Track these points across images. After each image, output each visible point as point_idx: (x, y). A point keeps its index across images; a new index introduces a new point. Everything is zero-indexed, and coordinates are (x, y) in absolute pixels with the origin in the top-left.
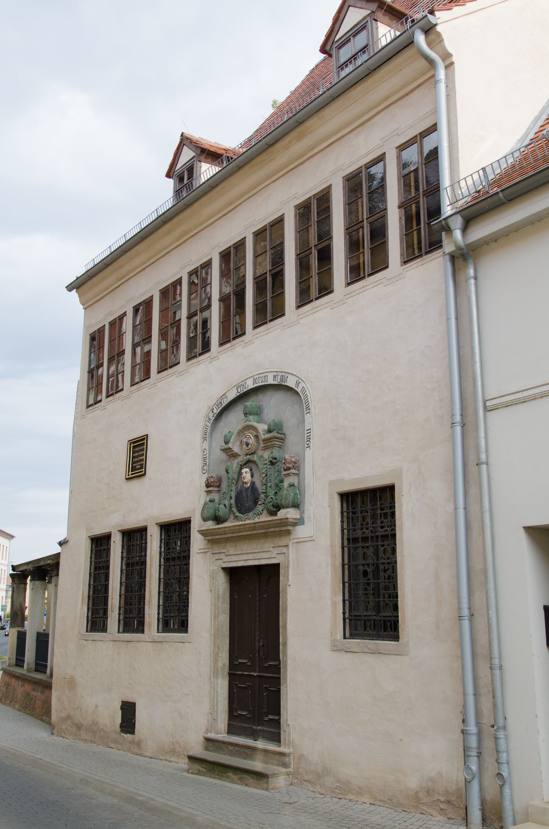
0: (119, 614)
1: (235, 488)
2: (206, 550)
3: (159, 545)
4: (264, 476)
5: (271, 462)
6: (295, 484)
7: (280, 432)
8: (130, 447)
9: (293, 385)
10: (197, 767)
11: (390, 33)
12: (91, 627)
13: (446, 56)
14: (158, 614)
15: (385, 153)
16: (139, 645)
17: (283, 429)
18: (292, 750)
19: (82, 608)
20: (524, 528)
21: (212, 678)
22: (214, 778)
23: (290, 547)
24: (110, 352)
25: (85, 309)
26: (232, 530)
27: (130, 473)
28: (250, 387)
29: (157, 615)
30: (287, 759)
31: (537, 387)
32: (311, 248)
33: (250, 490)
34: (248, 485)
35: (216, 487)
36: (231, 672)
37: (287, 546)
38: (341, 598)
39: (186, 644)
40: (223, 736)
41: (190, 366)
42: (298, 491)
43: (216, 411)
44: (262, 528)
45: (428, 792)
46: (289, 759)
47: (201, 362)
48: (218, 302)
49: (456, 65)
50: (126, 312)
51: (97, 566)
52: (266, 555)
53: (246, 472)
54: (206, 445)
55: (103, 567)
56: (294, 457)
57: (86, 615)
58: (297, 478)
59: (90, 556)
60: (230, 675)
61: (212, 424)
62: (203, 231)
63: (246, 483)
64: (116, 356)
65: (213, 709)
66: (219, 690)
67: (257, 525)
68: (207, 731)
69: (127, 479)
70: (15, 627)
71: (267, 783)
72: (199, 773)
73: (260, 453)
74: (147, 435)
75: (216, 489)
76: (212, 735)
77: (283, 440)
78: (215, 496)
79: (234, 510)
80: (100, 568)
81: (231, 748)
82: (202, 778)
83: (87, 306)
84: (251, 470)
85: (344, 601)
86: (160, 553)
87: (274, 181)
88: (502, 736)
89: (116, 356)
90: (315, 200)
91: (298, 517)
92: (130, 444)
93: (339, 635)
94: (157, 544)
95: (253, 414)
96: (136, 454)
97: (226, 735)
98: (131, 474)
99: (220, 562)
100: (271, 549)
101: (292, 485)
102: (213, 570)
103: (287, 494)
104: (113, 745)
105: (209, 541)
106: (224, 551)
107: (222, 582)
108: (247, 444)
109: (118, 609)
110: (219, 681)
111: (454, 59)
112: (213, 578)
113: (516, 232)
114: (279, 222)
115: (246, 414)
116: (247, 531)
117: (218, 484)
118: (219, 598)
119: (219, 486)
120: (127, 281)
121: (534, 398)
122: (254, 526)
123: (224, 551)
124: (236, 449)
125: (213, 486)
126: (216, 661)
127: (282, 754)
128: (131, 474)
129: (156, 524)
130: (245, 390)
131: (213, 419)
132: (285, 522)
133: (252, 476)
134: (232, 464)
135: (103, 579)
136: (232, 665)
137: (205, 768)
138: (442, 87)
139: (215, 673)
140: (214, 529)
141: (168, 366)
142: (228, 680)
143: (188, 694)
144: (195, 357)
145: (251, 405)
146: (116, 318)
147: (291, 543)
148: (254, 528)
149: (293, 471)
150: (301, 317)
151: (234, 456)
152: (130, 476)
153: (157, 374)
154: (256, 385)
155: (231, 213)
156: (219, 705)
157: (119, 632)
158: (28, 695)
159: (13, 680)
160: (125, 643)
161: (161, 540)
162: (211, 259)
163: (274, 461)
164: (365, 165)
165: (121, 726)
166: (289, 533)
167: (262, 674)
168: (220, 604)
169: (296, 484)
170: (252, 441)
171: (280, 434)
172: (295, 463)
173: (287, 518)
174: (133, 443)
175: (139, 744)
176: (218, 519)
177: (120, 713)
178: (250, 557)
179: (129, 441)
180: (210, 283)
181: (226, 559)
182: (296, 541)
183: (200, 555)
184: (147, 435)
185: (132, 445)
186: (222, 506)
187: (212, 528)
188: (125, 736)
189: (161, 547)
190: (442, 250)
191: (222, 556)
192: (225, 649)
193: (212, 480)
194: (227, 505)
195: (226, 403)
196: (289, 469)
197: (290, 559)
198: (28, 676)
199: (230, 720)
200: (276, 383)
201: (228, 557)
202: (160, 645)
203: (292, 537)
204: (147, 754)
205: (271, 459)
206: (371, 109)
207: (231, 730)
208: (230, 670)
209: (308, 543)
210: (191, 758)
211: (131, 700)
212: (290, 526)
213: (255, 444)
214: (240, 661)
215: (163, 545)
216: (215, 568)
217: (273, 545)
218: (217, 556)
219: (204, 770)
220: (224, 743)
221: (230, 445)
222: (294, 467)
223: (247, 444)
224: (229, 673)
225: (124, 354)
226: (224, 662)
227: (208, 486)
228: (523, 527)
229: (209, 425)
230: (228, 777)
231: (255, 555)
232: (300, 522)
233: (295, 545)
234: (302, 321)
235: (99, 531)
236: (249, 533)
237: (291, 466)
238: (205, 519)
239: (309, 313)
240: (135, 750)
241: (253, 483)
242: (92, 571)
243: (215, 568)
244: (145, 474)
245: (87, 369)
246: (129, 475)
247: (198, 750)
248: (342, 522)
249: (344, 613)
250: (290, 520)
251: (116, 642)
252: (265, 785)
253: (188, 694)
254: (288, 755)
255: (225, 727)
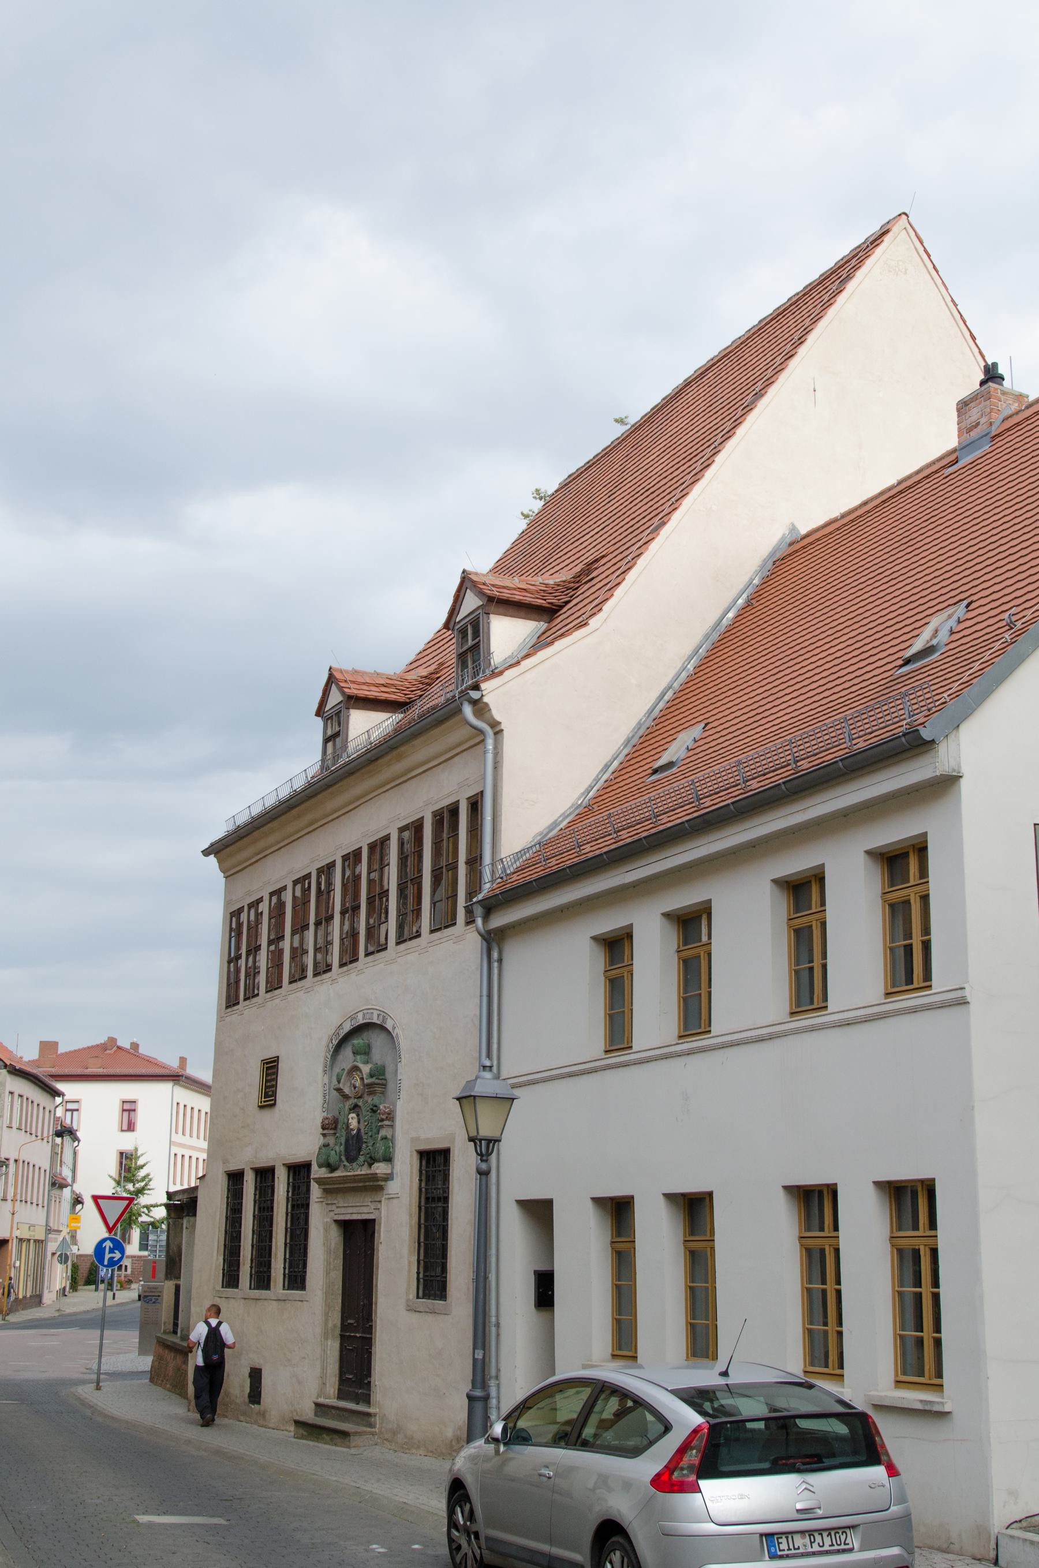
0: (251, 1267)
1: (345, 1133)
2: (322, 1200)
3: (286, 1190)
4: (366, 1124)
5: (372, 1109)
6: (388, 1137)
7: (381, 1077)
8: (263, 1068)
9: (390, 1028)
10: (301, 1431)
11: (250, 810)
12: (424, 1291)
13: (494, 724)
14: (285, 1268)
15: (459, 801)
16: (266, 1303)
17: (386, 1073)
18: (378, 1410)
19: (217, 1259)
20: (593, 1199)
21: (323, 1339)
22: (313, 1441)
23: (383, 1202)
24: (248, 944)
25: (226, 878)
26: (344, 1179)
27: (263, 1100)
28: (361, 1022)
29: (282, 1269)
30: (373, 1419)
31: (545, 1071)
32: (442, 867)
33: (355, 1138)
34: (355, 1132)
35: (331, 1129)
36: (342, 1333)
37: (380, 1202)
38: (416, 1258)
39: (305, 1302)
40: (333, 1401)
41: (316, 984)
42: (391, 1144)
43: (335, 1042)
44: (360, 1181)
45: (457, 1440)
46: (375, 1419)
47: (325, 981)
48: (339, 915)
49: (505, 733)
50: (262, 897)
51: (295, 1203)
52: (365, 1209)
53: (352, 1118)
54: (326, 1078)
55: (303, 1205)
56: (388, 1107)
57: (222, 1267)
58: (391, 1129)
59: (226, 1196)
60: (342, 1337)
61: (332, 1056)
62: (330, 824)
63: (352, 1130)
64: (253, 950)
65: (323, 1372)
66: (329, 1352)
67: (356, 1177)
68: (319, 1396)
69: (259, 1106)
70: (171, 1280)
71: (349, 1441)
72: (302, 1437)
73: (366, 1097)
74: (278, 1057)
75: (332, 1132)
76: (321, 1400)
77: (384, 1085)
78: (331, 1140)
79: (343, 1158)
80: (298, 1206)
81: (333, 1411)
82: (304, 1441)
83: (230, 873)
84: (358, 1115)
85: (419, 1261)
86: (288, 1199)
87: (385, 792)
88: (493, 1384)
89: (253, 950)
90: (413, 829)
91: (389, 1171)
92: (264, 1064)
93: (412, 1295)
94: (284, 1187)
95: (361, 1054)
96: (269, 1078)
97: (335, 1400)
98: (264, 1102)
99: (332, 1214)
100: (370, 1204)
101: (385, 1138)
102: (327, 1222)
103: (381, 1147)
104: (242, 1418)
105: (324, 1189)
106: (335, 1202)
107: (335, 1236)
108: (355, 1088)
109: (249, 1262)
110: (329, 1343)
111: (503, 727)
112: (326, 1231)
113: (845, 816)
114: (387, 838)
115: (354, 1053)
116: (350, 1183)
117: (333, 1126)
118: (330, 1253)
119: (335, 1128)
120: (265, 857)
121: (544, 1080)
122: (355, 1179)
123: (335, 1202)
124: (347, 1091)
125: (327, 1129)
126: (326, 1322)
127: (369, 1415)
128: (264, 1102)
129: (283, 1164)
130: (357, 1024)
131: (332, 1050)
132: (374, 1177)
133: (359, 1122)
134: (344, 1106)
135: (439, 1218)
136: (344, 1327)
137: (307, 1432)
138: (490, 757)
139: (326, 1335)
140: (325, 1178)
141: (443, 925)
142: (339, 1342)
143: (304, 1358)
144: (405, 941)
145: (359, 1044)
146: (349, 853)
147: (383, 1199)
148: (355, 1181)
149: (386, 1123)
150: (399, 955)
151: (346, 1097)
152: (263, 1104)
153: (430, 934)
154: (365, 1021)
155: (415, 779)
156: (328, 1368)
157: (250, 1288)
158: (179, 1369)
159: (167, 1351)
160: (255, 1301)
161: (288, 1184)
162: (423, 817)
163: (374, 1108)
164: (447, 806)
165: (250, 1396)
166: (381, 1188)
167: (364, 1335)
168: (332, 1260)
169: (389, 1137)
170: (358, 1083)
171: (381, 1079)
172: (389, 1114)
173: (376, 1174)
174: (267, 1063)
175: (263, 1414)
176: (332, 1168)
177: (248, 1381)
178: (354, 1210)
179: (262, 1061)
180: (334, 890)
181: (338, 1211)
182: (387, 1196)
183: (318, 1204)
184: (278, 1057)
185: (265, 1066)
186: (333, 1152)
187: (326, 1176)
188: (253, 1406)
189: (288, 1192)
190: (474, 925)
191: (334, 1207)
192: (337, 1308)
193: (327, 1122)
194: (338, 1152)
195: (343, 1035)
196: (382, 1120)
197: (383, 1215)
198: (179, 1345)
199: (340, 1385)
200: (379, 1023)
201: (339, 1209)
202: (282, 1303)
203: (385, 1192)
204: (270, 1426)
205: (371, 1107)
206: (446, 752)
207: (341, 1395)
208: (341, 1331)
209: (396, 1200)
210: (298, 1423)
211: (257, 1366)
212: (382, 1181)
213: (362, 1087)
214: (349, 1322)
215: (290, 1190)
216: (329, 1220)
217: (370, 1200)
218: (330, 1207)
219: (305, 1433)
220: (333, 1407)
221: (341, 1086)
222: (387, 1119)
223: (355, 1088)
224: (341, 1335)
225: (260, 950)
226: (335, 1323)
227: (323, 1128)
228: (783, 1187)
229: (329, 1057)
230: (323, 1439)
231: (358, 1208)
232: (389, 1177)
233: (387, 1201)
234: (399, 960)
235: (234, 1167)
236: (352, 1185)
237: (384, 1117)
238: (320, 1166)
239: (403, 954)
240: (261, 1422)
241: (359, 1130)
242: (423, 1203)
243: (329, 1220)
244: (274, 1105)
245: (226, 958)
246: (261, 1102)
247: (308, 1414)
248: (420, 1180)
249: (418, 1273)
250: (379, 1175)
251: (247, 1300)
252: (348, 1443)
253: (304, 1358)
254: (375, 1415)
255: (334, 1391)
